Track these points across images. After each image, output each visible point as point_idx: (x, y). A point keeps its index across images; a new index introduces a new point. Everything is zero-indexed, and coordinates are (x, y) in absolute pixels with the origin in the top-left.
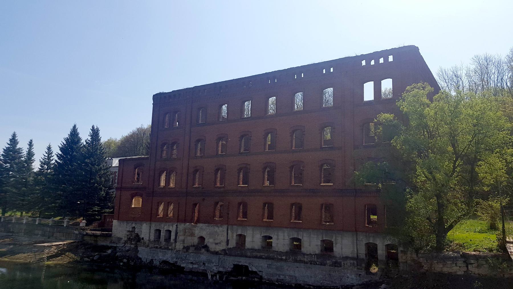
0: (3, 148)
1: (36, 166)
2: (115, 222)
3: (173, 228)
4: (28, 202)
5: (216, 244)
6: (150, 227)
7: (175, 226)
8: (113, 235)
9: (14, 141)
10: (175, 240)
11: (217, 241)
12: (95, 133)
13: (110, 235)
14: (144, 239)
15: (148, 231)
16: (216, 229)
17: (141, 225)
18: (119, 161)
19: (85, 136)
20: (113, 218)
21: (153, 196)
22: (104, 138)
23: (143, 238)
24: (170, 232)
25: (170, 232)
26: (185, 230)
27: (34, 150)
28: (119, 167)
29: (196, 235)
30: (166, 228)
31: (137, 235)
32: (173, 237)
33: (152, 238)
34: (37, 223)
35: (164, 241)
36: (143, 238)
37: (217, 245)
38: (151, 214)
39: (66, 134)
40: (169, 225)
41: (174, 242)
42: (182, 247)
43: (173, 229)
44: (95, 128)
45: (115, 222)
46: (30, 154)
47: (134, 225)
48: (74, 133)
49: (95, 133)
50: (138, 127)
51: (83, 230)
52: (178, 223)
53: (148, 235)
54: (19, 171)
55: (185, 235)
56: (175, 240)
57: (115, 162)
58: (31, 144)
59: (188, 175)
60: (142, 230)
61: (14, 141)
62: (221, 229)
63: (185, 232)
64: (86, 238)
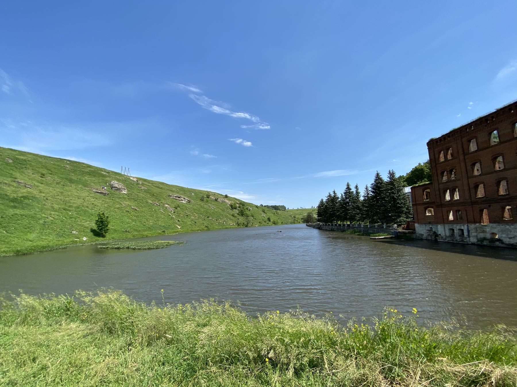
0: (350, 184)
1: (362, 198)
2: (416, 225)
3: (465, 228)
4: (482, 211)
5: (510, 238)
6: (444, 227)
7: (466, 226)
8: (416, 233)
9: (348, 188)
10: (469, 236)
11: (510, 236)
12: (392, 175)
13: (415, 233)
14: (441, 234)
15: (443, 230)
16: (508, 227)
17: (437, 226)
18: (411, 188)
19: (385, 178)
20: (414, 222)
21: (442, 207)
22: (397, 176)
23: (440, 235)
24: (462, 230)
25: (462, 230)
26: (476, 228)
27: (359, 191)
28: (412, 192)
29: (487, 232)
30: (458, 227)
31: (435, 232)
32: (466, 233)
33: (448, 234)
34: (369, 227)
35: (458, 236)
36: (440, 235)
37: (511, 239)
38: (443, 219)
39: (372, 181)
40: (460, 226)
41: (467, 237)
42: (476, 241)
43: (465, 228)
44: (391, 172)
45: (416, 225)
46: (358, 193)
47: (431, 226)
48: (378, 178)
49: (392, 175)
50: (416, 166)
51: (396, 229)
52: (469, 224)
53: (443, 233)
54: (354, 202)
55: (477, 232)
56: (469, 236)
57: (408, 190)
58: (357, 187)
59: (470, 190)
60: (439, 229)
61: (348, 188)
62: (512, 227)
63: (477, 230)
64: (399, 234)
